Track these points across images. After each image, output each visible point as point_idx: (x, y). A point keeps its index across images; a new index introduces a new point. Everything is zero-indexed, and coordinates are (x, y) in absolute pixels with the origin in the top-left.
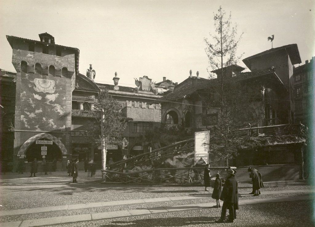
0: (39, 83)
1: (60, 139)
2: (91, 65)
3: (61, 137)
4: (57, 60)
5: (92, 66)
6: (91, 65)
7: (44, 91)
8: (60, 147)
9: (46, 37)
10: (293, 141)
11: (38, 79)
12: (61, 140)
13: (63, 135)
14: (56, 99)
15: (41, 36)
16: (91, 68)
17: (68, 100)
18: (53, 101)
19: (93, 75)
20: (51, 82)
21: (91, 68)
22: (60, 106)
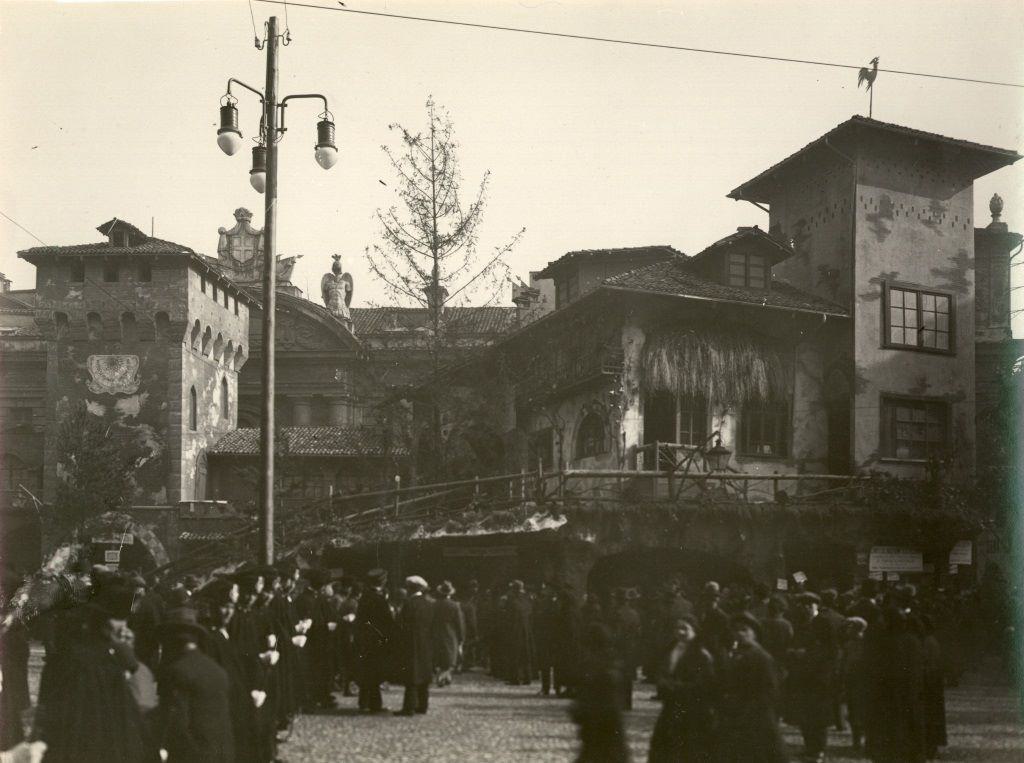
0: (99, 368)
1: (152, 527)
2: (337, 257)
3: (155, 523)
4: (140, 296)
5: (341, 261)
6: (337, 257)
7: (112, 388)
8: (152, 551)
9: (117, 230)
10: (493, 529)
11: (96, 358)
12: (154, 531)
13: (160, 517)
14: (142, 408)
15: (103, 229)
16: (336, 268)
17: (173, 410)
18: (135, 416)
19: (343, 293)
20: (128, 361)
21: (336, 268)
22: (152, 428)
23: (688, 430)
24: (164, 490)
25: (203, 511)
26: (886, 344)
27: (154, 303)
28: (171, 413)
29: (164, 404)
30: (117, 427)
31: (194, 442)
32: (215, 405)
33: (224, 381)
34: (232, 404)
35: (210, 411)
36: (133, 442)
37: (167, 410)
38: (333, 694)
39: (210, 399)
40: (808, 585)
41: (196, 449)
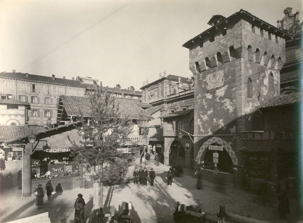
3: (231, 141)
12: (231, 145)
17: (238, 90)
18: (222, 96)
24: (235, 126)
27: (228, 44)
29: (234, 88)
30: (216, 102)
31: (251, 104)
32: (265, 86)
33: (271, 74)
34: (276, 85)
35: (262, 88)
37: (235, 91)
39: (262, 83)
40: (204, 164)
41: (252, 107)
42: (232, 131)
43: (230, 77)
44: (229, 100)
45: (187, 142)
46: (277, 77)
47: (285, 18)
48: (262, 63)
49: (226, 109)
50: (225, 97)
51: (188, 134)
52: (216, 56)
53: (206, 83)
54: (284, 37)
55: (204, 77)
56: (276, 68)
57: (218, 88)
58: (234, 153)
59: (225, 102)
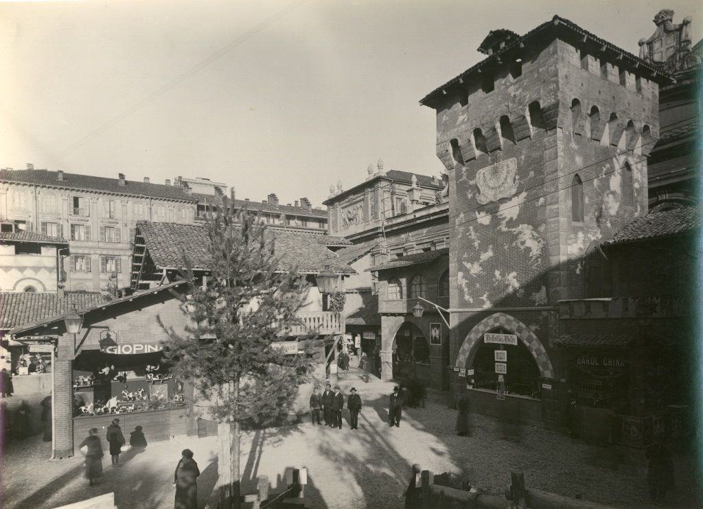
1: (533, 328)
8: (534, 353)
12: (536, 332)
17: (551, 204)
23: (126, 295)
24: (544, 288)
25: (584, 311)
26: (88, 228)
27: (525, 96)
28: (548, 207)
30: (500, 232)
31: (581, 235)
32: (613, 193)
33: (627, 166)
35: (606, 199)
36: (514, 244)
37: (544, 206)
38: (358, 335)
42: (537, 299)
43: (532, 173)
44: (531, 227)
45: (433, 326)
46: (641, 171)
47: (657, 36)
48: (606, 140)
49: (522, 247)
50: (521, 220)
51: (437, 306)
52: (498, 125)
53: (476, 189)
54: (654, 80)
55: (472, 175)
56: (638, 151)
57: (503, 200)
58: (544, 350)
59: (520, 233)
